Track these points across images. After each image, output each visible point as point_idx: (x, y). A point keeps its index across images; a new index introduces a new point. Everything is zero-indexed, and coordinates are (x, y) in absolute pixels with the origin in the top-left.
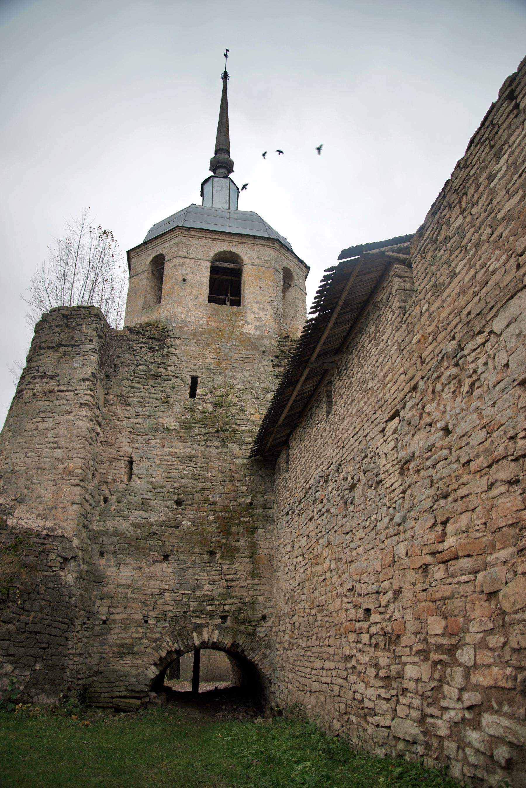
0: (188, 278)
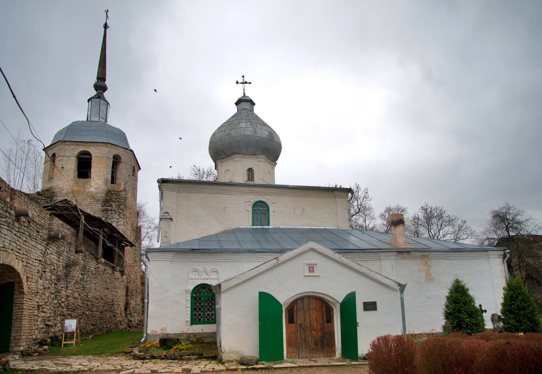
0: (64, 166)
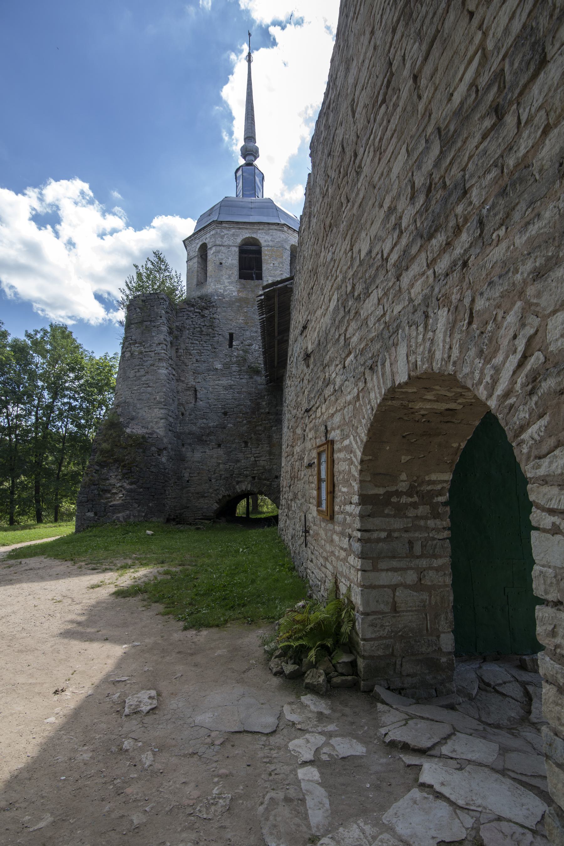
0: (223, 262)
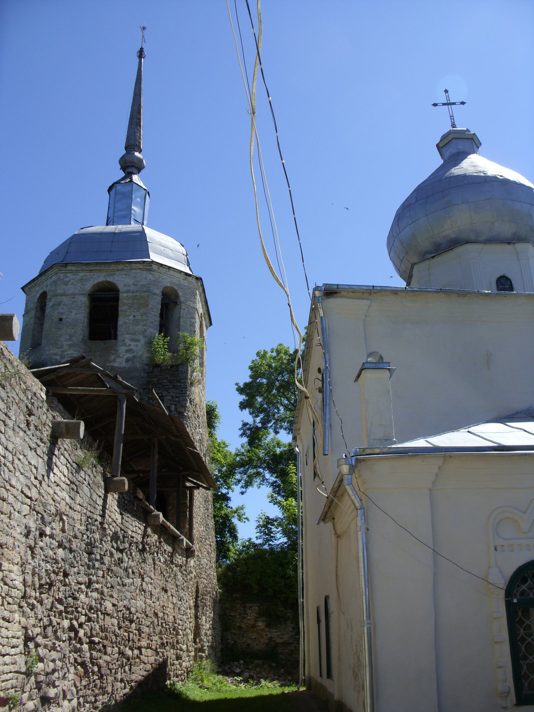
0: (64, 317)
